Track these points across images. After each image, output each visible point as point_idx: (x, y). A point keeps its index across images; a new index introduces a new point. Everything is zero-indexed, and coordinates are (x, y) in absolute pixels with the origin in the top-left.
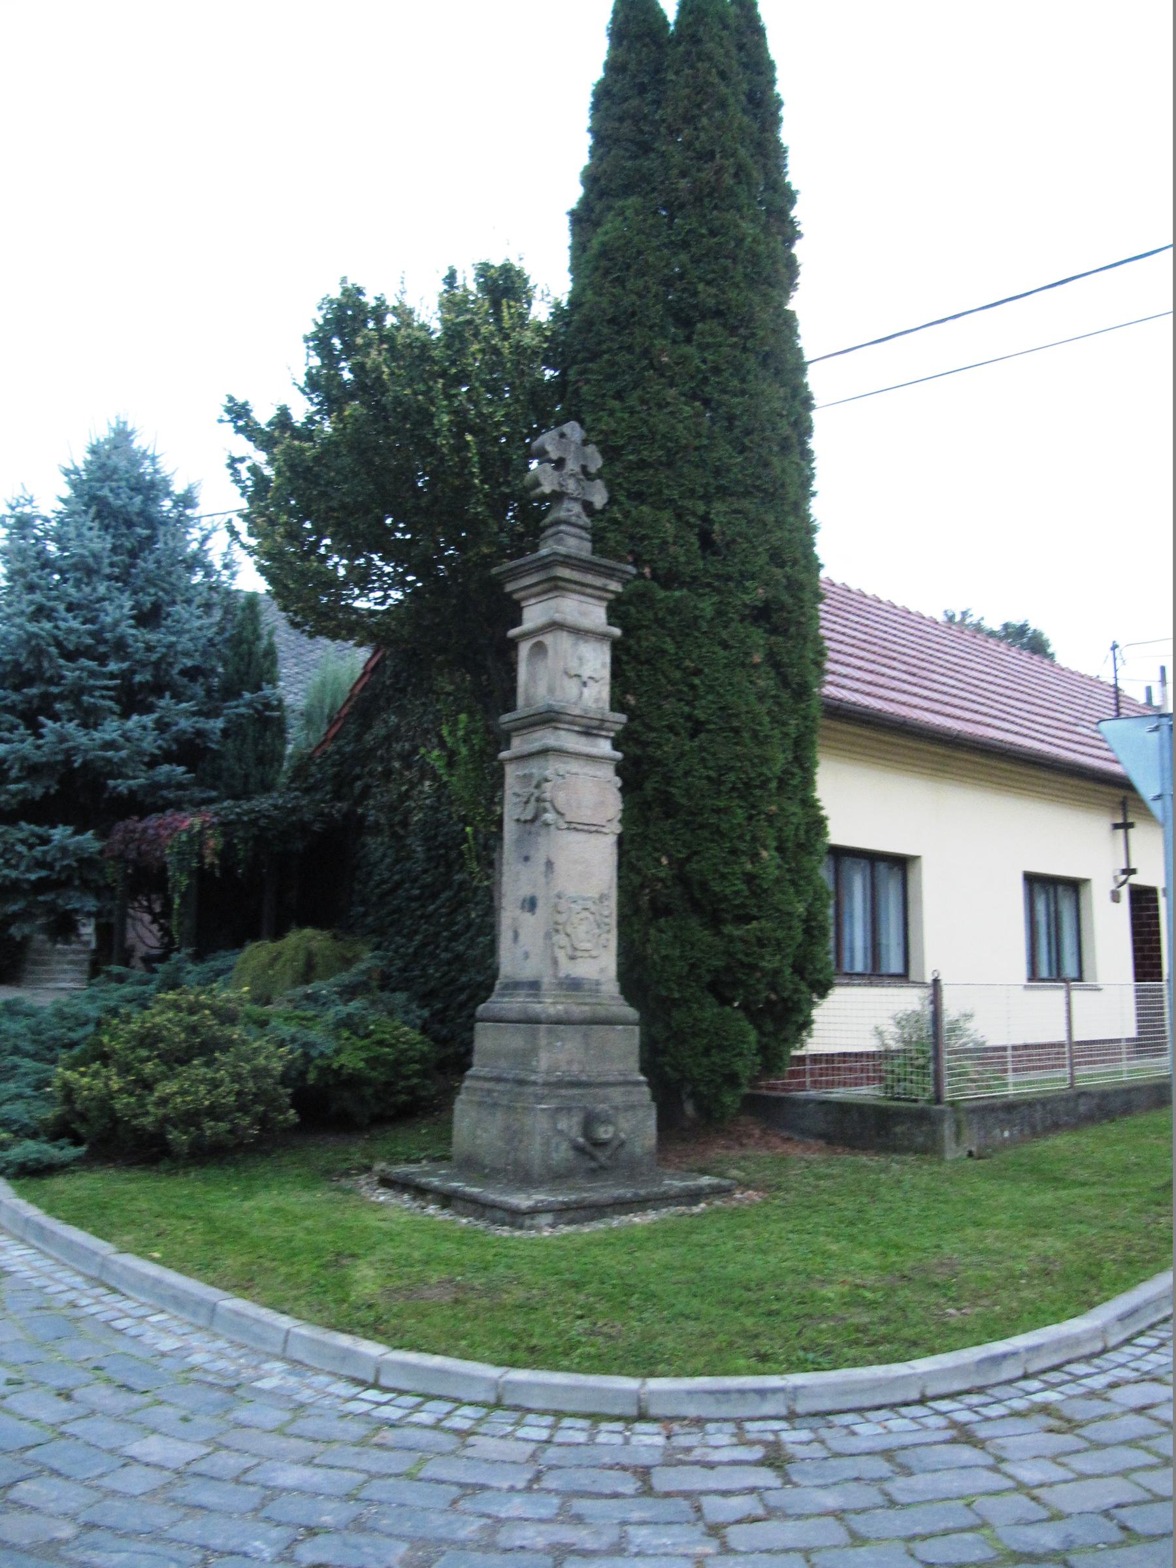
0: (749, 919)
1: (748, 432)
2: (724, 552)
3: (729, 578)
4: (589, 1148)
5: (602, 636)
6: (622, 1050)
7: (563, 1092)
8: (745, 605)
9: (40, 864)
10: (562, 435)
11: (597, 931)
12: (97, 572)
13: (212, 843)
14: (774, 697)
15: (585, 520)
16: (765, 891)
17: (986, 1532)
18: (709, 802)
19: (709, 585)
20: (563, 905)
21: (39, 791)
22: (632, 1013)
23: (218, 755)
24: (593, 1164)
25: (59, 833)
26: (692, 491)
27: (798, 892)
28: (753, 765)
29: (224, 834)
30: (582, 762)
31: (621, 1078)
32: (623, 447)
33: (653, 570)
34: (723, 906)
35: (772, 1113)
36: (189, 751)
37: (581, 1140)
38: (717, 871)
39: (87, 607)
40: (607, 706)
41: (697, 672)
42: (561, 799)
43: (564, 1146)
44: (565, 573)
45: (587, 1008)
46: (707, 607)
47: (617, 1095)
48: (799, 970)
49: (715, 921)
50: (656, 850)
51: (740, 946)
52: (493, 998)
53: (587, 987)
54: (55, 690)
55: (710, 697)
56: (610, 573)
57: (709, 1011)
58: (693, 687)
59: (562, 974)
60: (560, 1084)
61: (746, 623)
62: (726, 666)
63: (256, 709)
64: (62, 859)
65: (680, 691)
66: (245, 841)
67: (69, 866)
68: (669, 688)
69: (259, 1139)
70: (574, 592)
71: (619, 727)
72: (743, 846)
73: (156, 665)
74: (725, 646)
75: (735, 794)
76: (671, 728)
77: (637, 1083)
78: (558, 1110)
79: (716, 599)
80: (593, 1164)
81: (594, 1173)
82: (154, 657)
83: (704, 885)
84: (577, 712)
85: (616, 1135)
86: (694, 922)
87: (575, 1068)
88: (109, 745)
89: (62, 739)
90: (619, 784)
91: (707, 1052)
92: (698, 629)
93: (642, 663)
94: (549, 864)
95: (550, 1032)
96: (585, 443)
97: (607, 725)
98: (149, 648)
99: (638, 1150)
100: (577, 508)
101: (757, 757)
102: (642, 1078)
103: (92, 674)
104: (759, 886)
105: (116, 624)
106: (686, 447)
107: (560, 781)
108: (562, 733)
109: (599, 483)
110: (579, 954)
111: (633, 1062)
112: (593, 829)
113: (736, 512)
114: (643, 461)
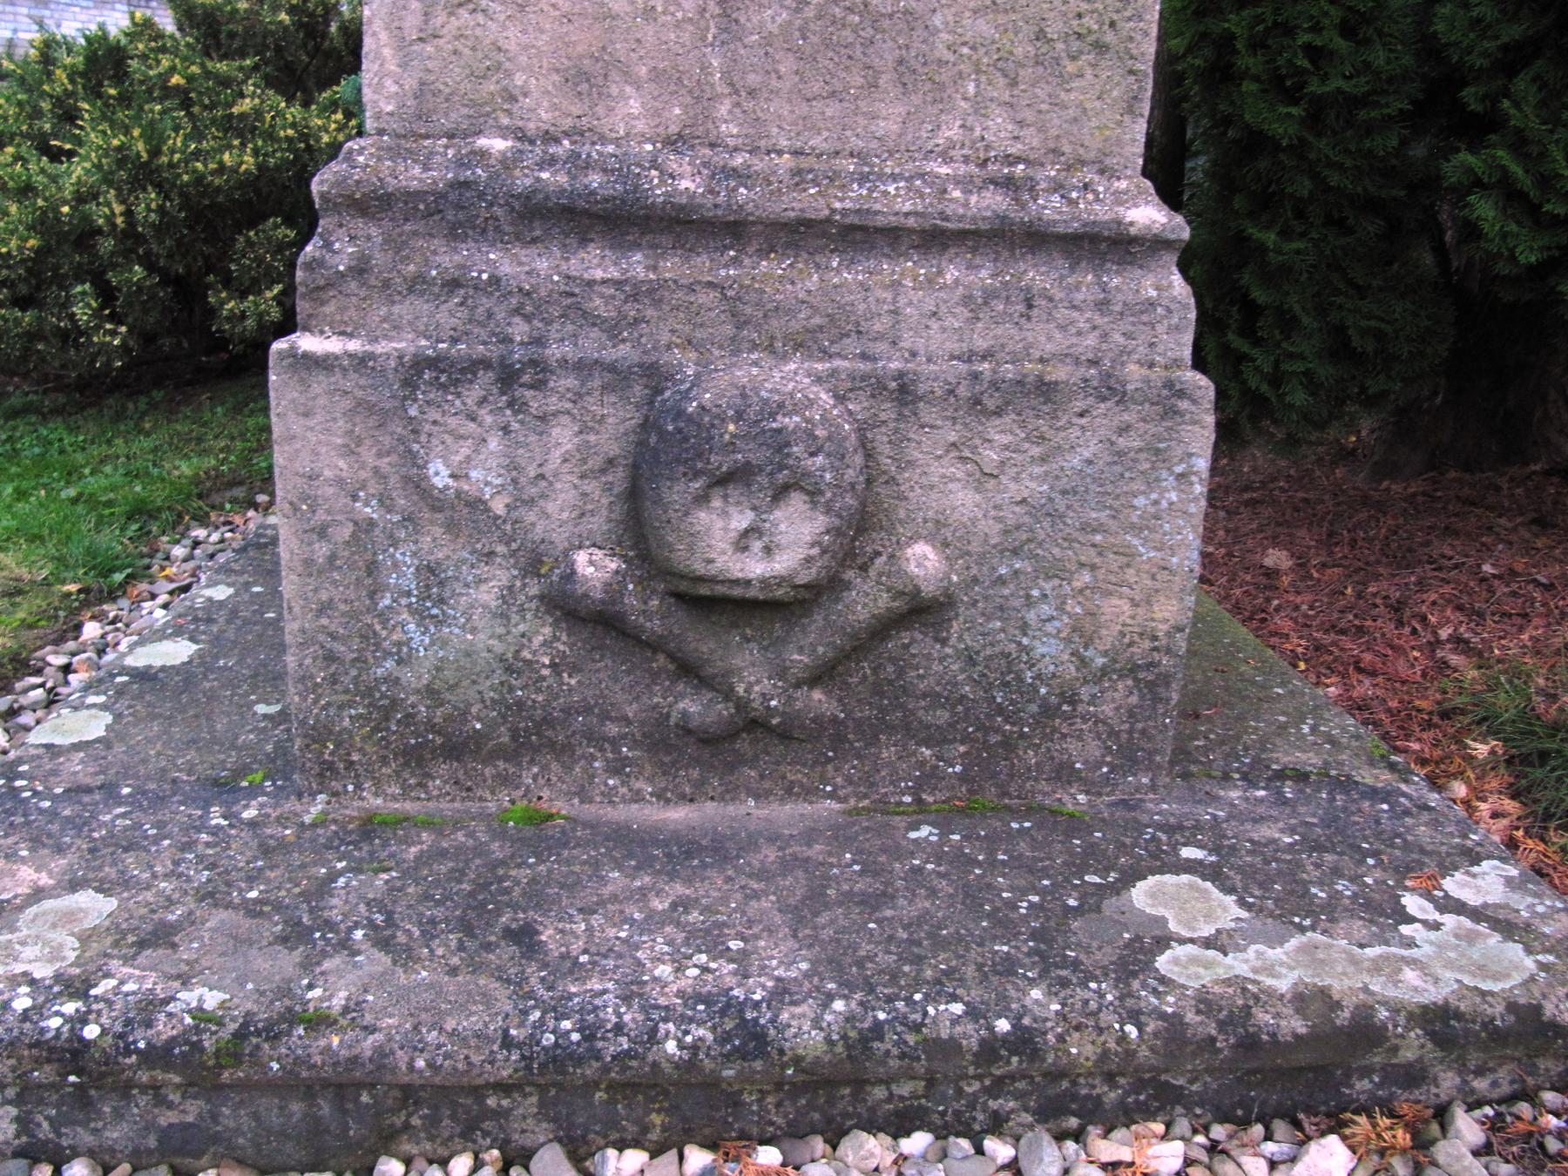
4: (647, 610)
17: (1470, 1100)
24: (692, 706)
31: (992, 202)
37: (594, 568)
43: (486, 589)
47: (928, 315)
77: (1112, 246)
78: (431, 373)
80: (692, 706)
87: (631, 113)
99: (1049, 650)
111: (1112, 113)
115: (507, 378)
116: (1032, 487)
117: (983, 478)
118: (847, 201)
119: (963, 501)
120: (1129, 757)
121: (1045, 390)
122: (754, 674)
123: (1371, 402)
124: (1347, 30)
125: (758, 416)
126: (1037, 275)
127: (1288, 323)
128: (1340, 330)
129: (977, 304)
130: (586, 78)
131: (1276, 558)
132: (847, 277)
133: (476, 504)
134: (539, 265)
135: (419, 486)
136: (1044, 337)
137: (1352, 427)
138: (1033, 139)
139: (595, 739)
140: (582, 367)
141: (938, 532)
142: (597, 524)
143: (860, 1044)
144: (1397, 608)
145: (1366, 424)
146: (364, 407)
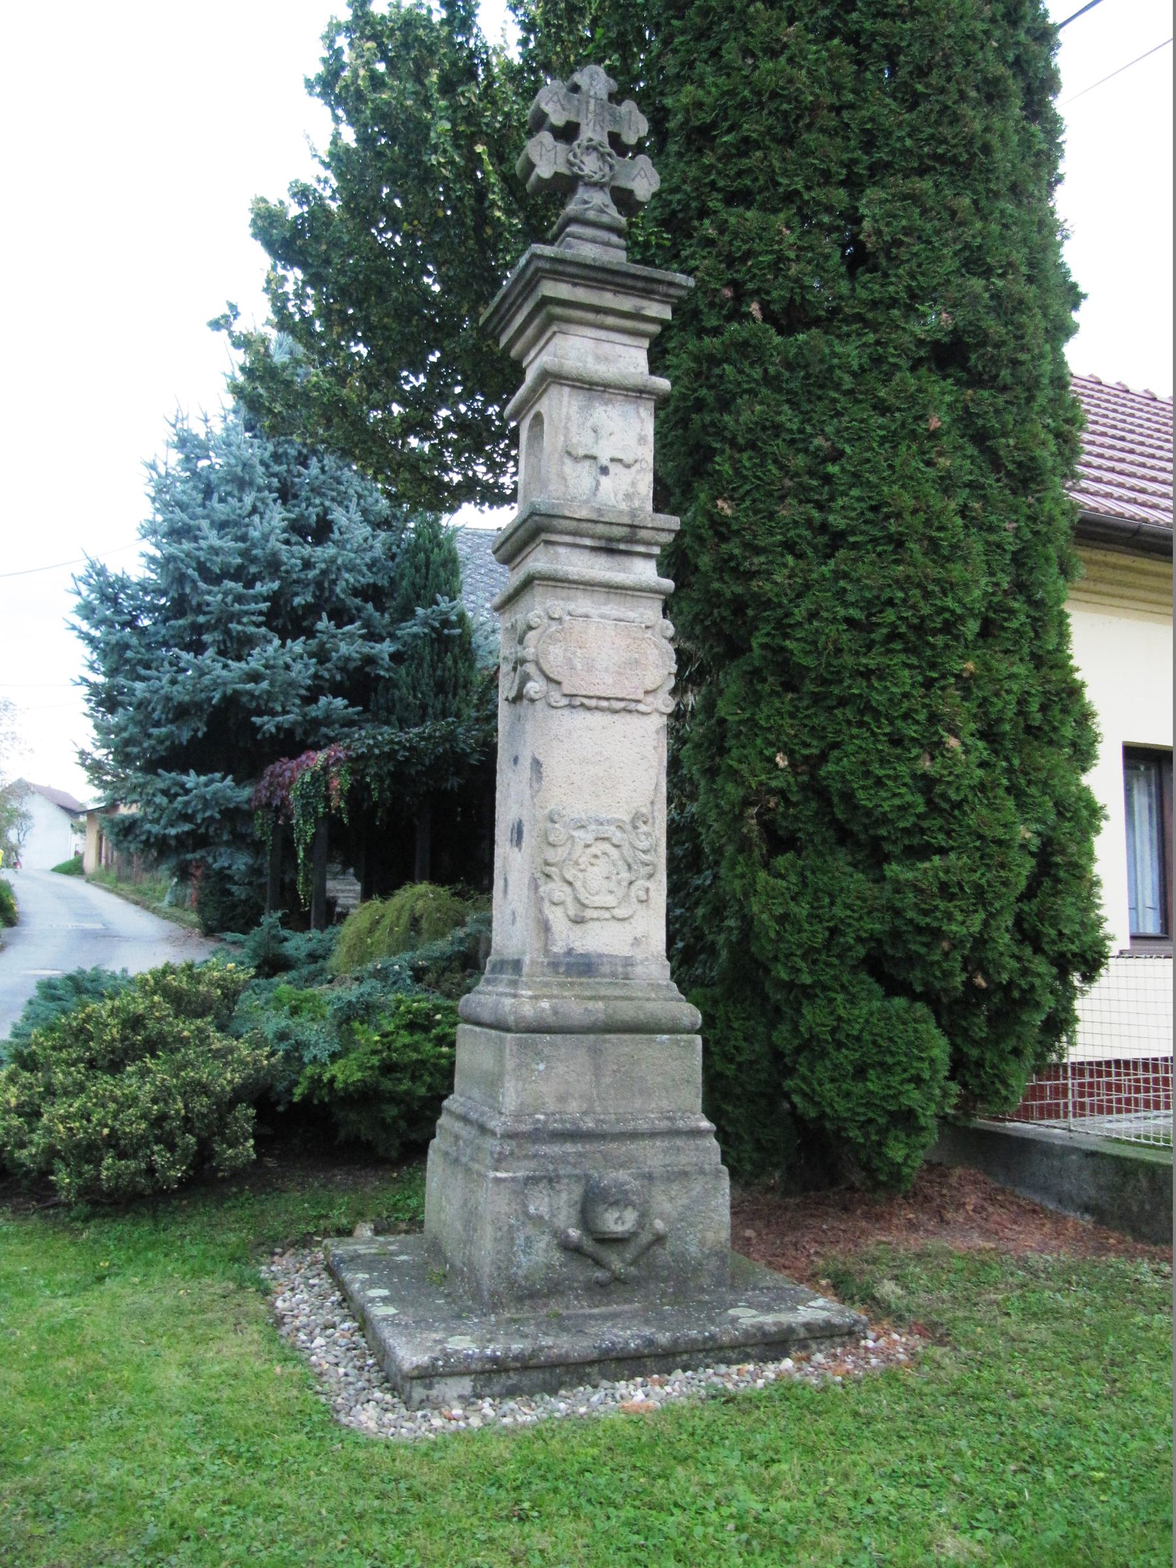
0: (924, 852)
1: (922, 72)
2: (883, 262)
3: (894, 302)
4: (589, 1245)
5: (638, 393)
6: (670, 1078)
7: (544, 1149)
8: (920, 343)
9: (185, 817)
10: (575, 88)
11: (625, 875)
12: (251, 483)
13: (335, 783)
14: (970, 485)
15: (614, 215)
16: (958, 805)
18: (849, 660)
19: (859, 318)
20: (559, 833)
21: (186, 736)
22: (690, 1014)
23: (390, 684)
24: (599, 1274)
25: (191, 779)
26: (827, 175)
27: (1021, 806)
28: (927, 595)
29: (352, 772)
30: (601, 597)
31: (665, 1125)
32: (714, 125)
33: (764, 308)
34: (883, 832)
35: (1005, 1162)
36: (360, 684)
37: (574, 1233)
38: (867, 774)
39: (236, 524)
40: (649, 506)
41: (837, 456)
42: (555, 658)
43: (543, 1242)
44: (562, 290)
45: (600, 1005)
46: (852, 352)
47: (654, 1155)
48: (1028, 935)
49: (874, 857)
50: (770, 744)
51: (911, 898)
52: (481, 987)
53: (606, 969)
54: (201, 619)
55: (855, 492)
56: (647, 289)
57: (868, 1007)
58: (827, 479)
59: (558, 948)
60: (537, 1135)
61: (923, 371)
62: (883, 440)
63: (433, 629)
64: (204, 810)
65: (807, 489)
66: (378, 777)
67: (211, 818)
68: (788, 483)
69: (186, 1185)
70: (569, 321)
71: (668, 538)
72: (911, 731)
73: (319, 584)
74: (882, 408)
75: (897, 646)
76: (789, 546)
77: (697, 1133)
78: (531, 1180)
79: (871, 338)
80: (599, 1274)
81: (602, 1289)
82: (312, 574)
83: (848, 797)
84: (583, 513)
85: (641, 1224)
86: (841, 860)
88: (255, 677)
89: (202, 673)
90: (671, 631)
91: (860, 1073)
92: (837, 387)
93: (741, 450)
94: (537, 764)
95: (522, 1045)
96: (615, 98)
97: (643, 534)
98: (307, 564)
99: (693, 1249)
100: (600, 198)
101: (936, 581)
102: (705, 1124)
103: (239, 599)
104: (944, 796)
105: (266, 537)
106: (814, 108)
107: (554, 627)
108: (562, 550)
109: (643, 160)
110: (589, 913)
111: (693, 1097)
112: (625, 707)
113: (905, 197)
114: (746, 140)
115: (550, 1180)
116: (685, 1201)
117: (671, 1199)
118: (630, 1126)
119: (667, 1207)
120: (719, 1284)
121: (685, 1174)
122: (617, 1262)
123: (776, 1166)
124: (745, 1039)
125: (619, 1185)
126: (679, 1142)
127: (739, 1137)
128: (758, 1141)
129: (665, 1152)
130: (562, 1099)
131: (749, 1233)
132: (632, 1147)
133: (541, 1217)
134: (555, 1149)
135: (526, 1213)
136: (683, 1159)
137: (771, 1175)
138: (673, 1106)
139: (571, 1288)
140: (569, 1176)
141: (661, 1216)
142: (573, 1221)
143: (675, 1341)
144: (795, 1245)
145: (777, 1174)
146: (514, 1192)
